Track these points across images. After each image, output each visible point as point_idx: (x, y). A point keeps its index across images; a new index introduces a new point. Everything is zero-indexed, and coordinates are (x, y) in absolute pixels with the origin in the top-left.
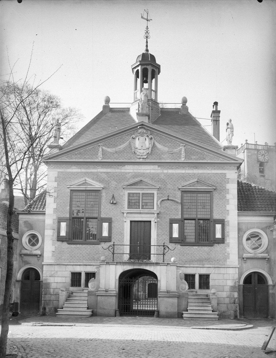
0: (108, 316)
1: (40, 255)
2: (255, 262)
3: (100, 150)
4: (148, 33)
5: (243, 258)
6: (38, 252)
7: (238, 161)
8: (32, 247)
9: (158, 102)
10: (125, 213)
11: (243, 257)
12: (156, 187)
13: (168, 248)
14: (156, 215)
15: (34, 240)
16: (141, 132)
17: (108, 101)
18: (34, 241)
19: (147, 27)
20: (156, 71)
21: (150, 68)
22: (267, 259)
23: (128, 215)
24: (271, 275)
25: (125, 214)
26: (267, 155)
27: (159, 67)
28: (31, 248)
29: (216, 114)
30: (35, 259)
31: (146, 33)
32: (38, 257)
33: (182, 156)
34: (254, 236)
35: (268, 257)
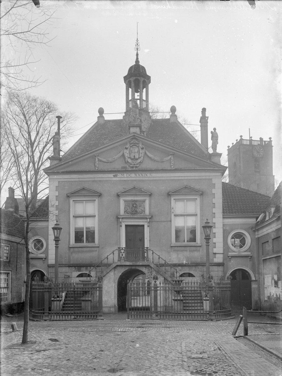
0: (109, 314)
1: (45, 258)
2: (239, 260)
4: (138, 45)
5: (228, 257)
6: (43, 256)
8: (37, 251)
15: (39, 244)
17: (101, 111)
18: (39, 246)
19: (137, 39)
22: (43, 259)
23: (123, 220)
24: (254, 271)
26: (262, 150)
28: (37, 252)
29: (204, 120)
30: (41, 261)
31: (136, 45)
32: (43, 260)
34: (238, 236)
35: (251, 255)
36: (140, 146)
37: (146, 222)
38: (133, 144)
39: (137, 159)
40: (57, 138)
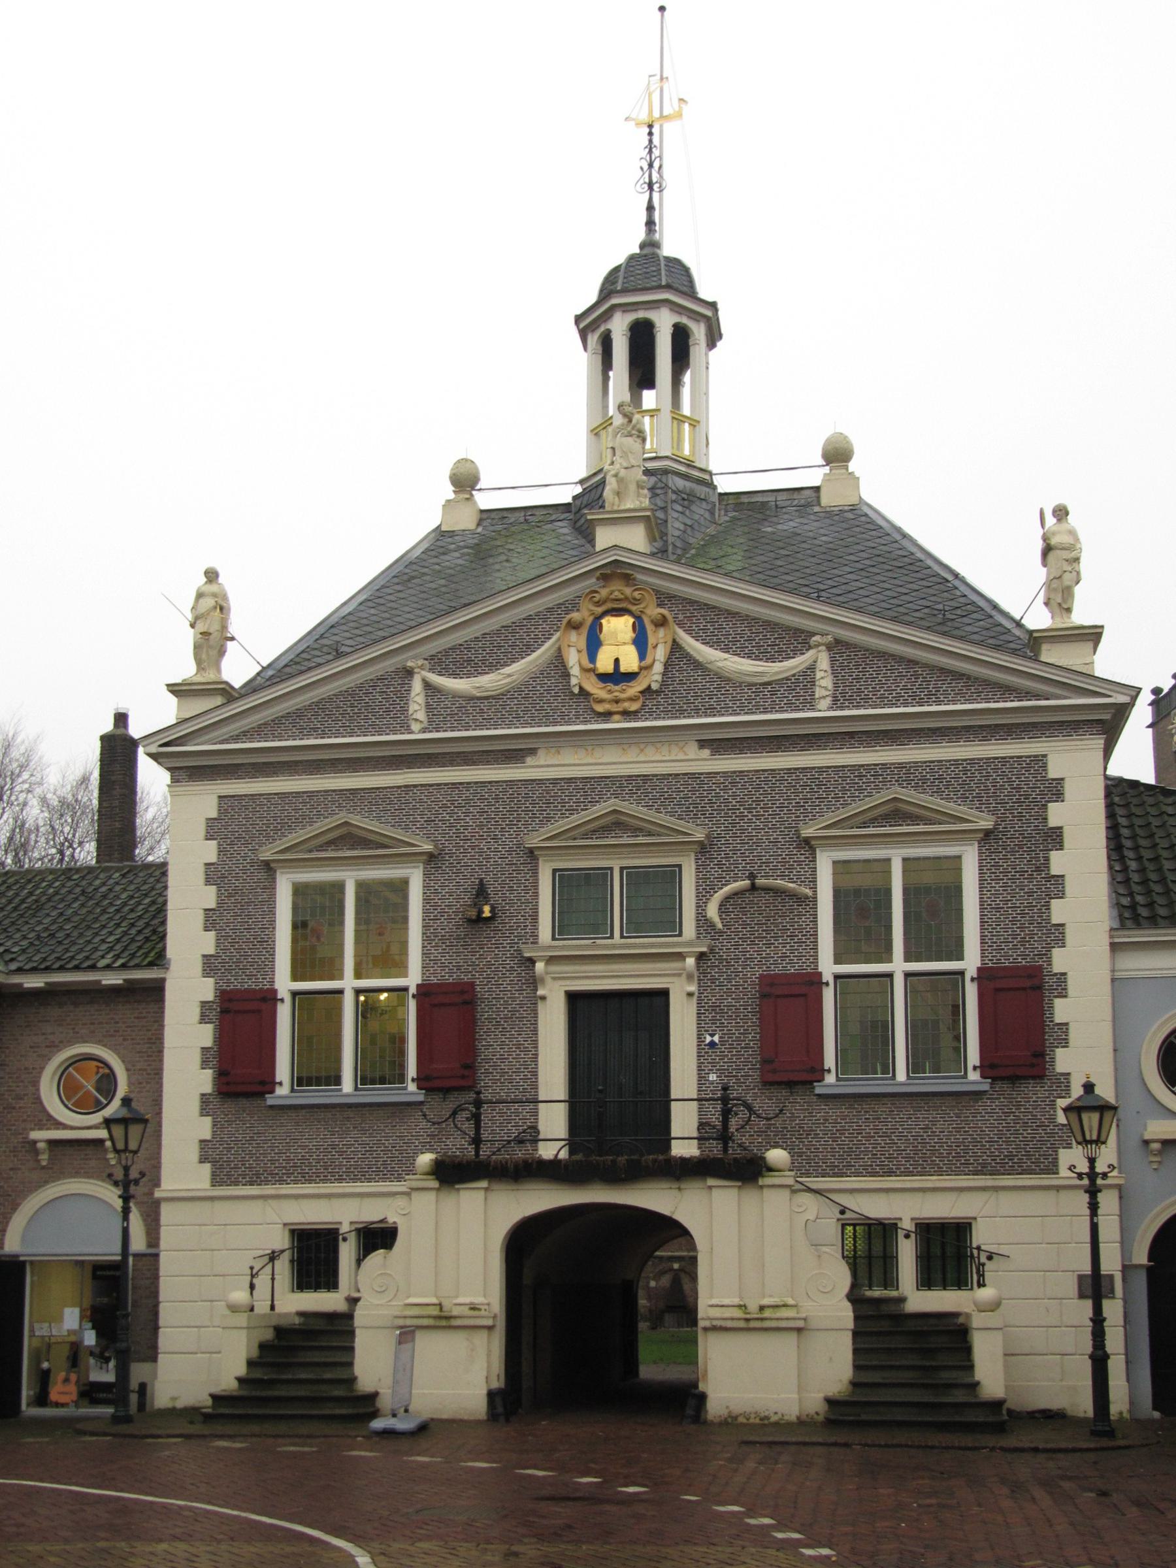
3: (417, 686)
5: (1146, 1143)
7: (1110, 696)
9: (713, 468)
10: (541, 958)
11: (1146, 1137)
12: (681, 839)
13: (749, 1108)
14: (691, 961)
16: (612, 597)
20: (698, 332)
21: (664, 323)
23: (555, 968)
25: (540, 966)
27: (709, 313)
31: (646, 167)
33: (819, 692)
36: (648, 611)
37: (679, 975)
38: (609, 605)
39: (631, 676)
40: (214, 595)
